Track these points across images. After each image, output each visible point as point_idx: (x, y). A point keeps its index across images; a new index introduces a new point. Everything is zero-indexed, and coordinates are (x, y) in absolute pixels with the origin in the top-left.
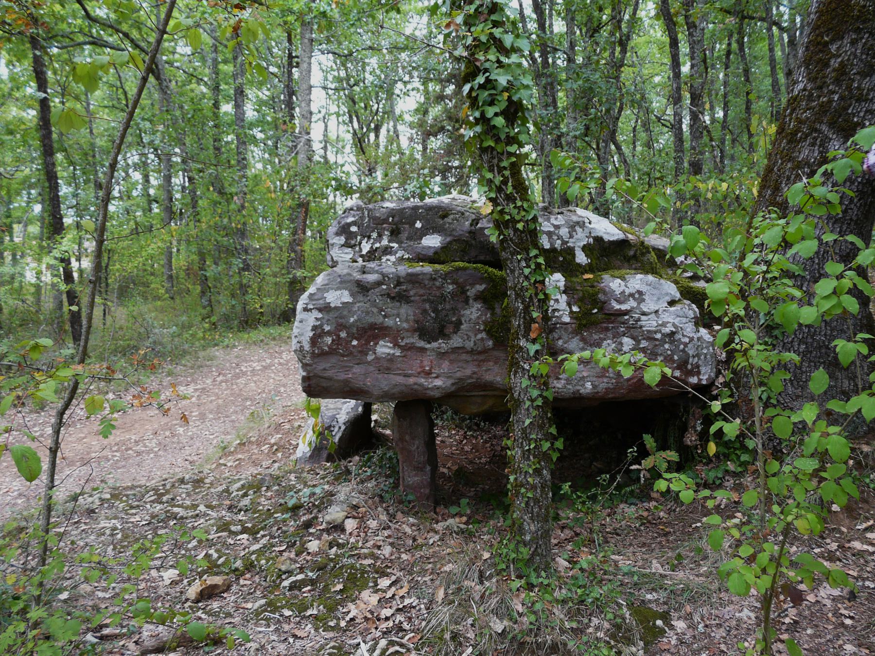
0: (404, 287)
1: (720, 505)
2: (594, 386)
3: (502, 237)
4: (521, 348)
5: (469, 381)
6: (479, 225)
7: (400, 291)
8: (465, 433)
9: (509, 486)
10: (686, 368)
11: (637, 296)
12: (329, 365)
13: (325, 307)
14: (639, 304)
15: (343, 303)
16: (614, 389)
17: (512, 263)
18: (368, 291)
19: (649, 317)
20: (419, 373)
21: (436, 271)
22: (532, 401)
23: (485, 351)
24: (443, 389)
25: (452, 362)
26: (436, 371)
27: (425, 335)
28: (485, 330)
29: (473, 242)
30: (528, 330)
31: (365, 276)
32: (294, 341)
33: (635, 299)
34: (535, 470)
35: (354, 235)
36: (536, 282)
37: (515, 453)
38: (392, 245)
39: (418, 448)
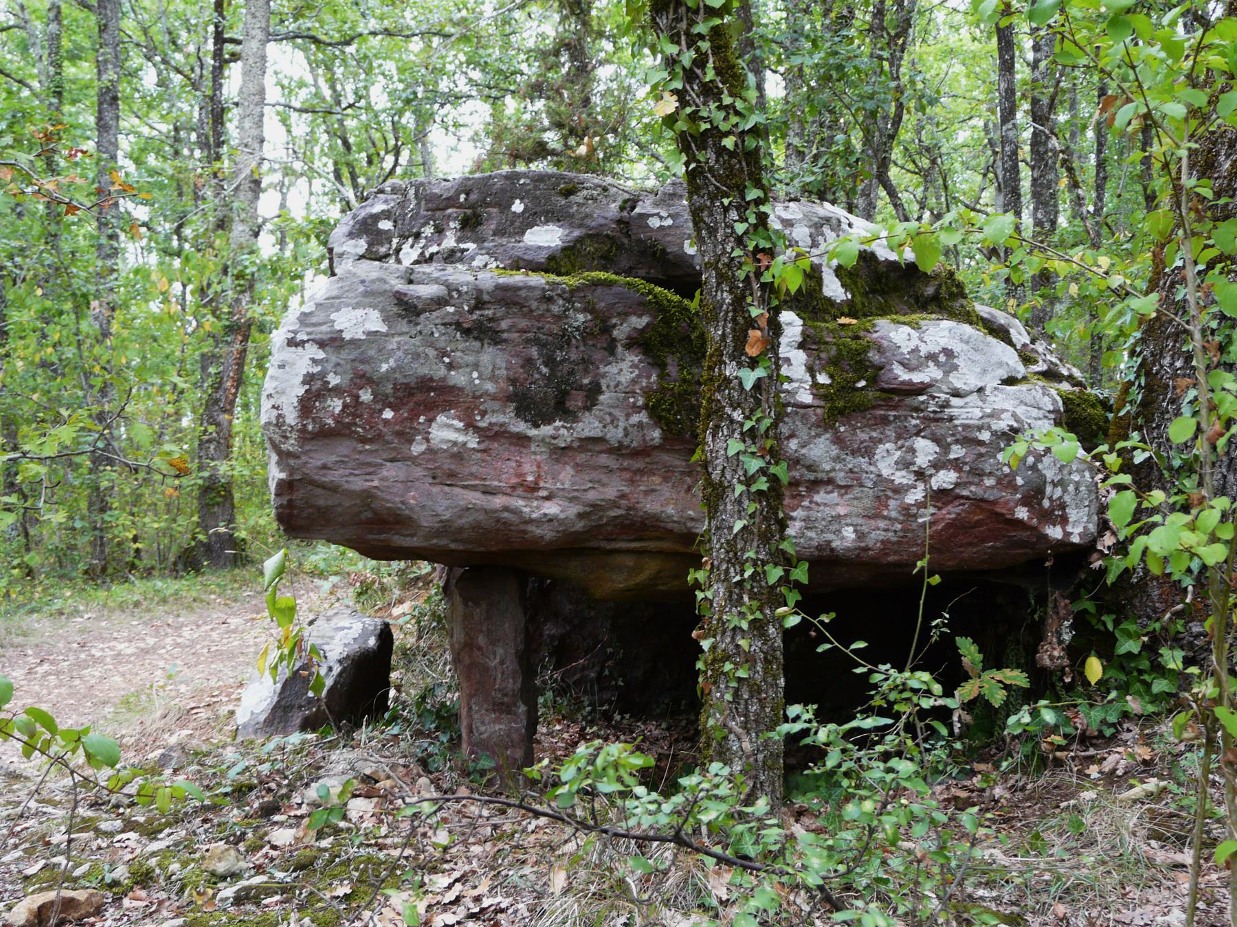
0: (489, 313)
1: (1115, 770)
2: (861, 536)
3: (693, 166)
4: (727, 381)
5: (612, 514)
6: (637, 210)
7: (480, 319)
8: (583, 729)
9: (700, 665)
10: (1040, 504)
11: (942, 358)
12: (334, 458)
13: (333, 340)
14: (947, 373)
15: (369, 333)
16: (898, 543)
17: (711, 215)
18: (418, 315)
19: (967, 399)
20: (514, 488)
21: (554, 285)
22: (749, 481)
23: (644, 451)
24: (561, 522)
25: (579, 468)
26: (548, 484)
27: (528, 408)
28: (646, 407)
29: (625, 241)
30: (741, 340)
31: (412, 287)
32: (266, 405)
33: (938, 364)
34: (753, 623)
35: (385, 237)
36: (757, 249)
37: (713, 594)
38: (462, 246)
39: (502, 662)
